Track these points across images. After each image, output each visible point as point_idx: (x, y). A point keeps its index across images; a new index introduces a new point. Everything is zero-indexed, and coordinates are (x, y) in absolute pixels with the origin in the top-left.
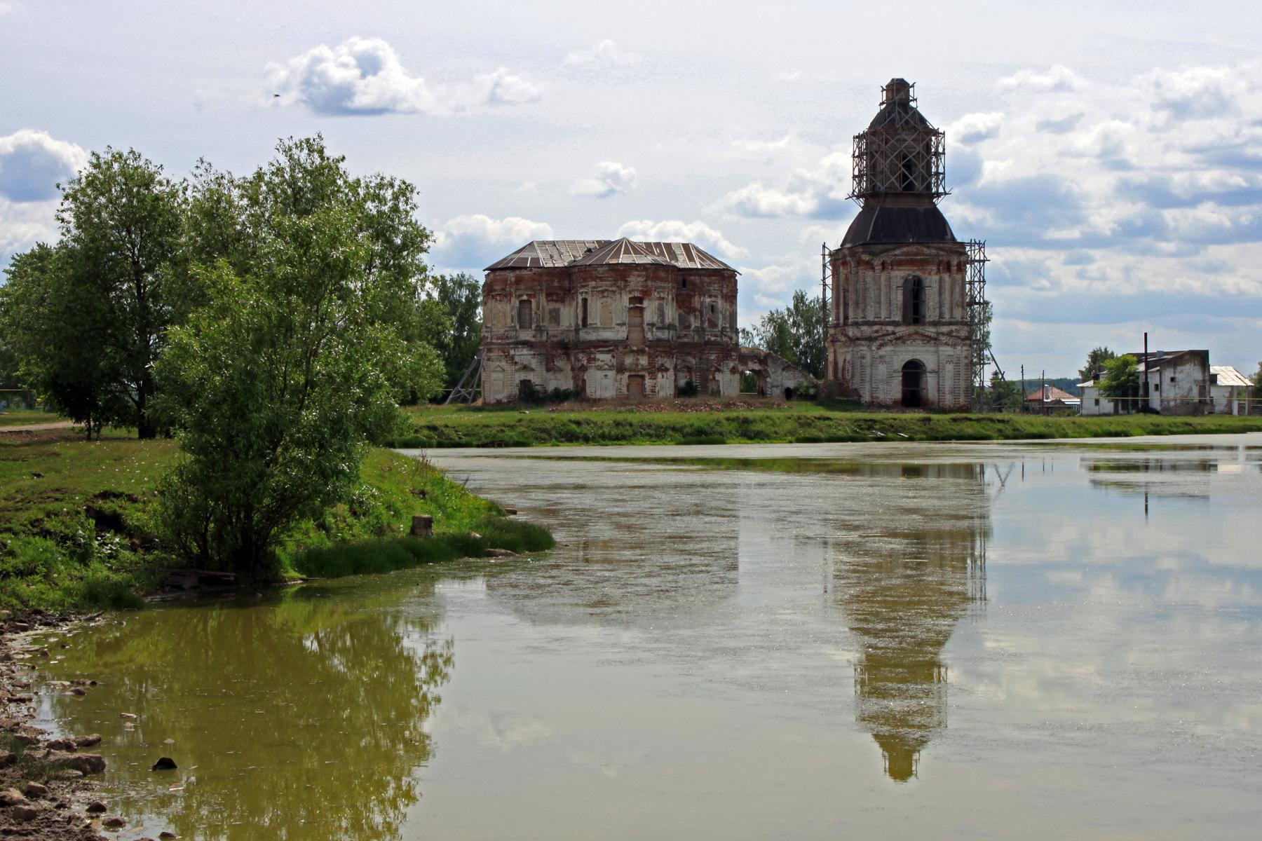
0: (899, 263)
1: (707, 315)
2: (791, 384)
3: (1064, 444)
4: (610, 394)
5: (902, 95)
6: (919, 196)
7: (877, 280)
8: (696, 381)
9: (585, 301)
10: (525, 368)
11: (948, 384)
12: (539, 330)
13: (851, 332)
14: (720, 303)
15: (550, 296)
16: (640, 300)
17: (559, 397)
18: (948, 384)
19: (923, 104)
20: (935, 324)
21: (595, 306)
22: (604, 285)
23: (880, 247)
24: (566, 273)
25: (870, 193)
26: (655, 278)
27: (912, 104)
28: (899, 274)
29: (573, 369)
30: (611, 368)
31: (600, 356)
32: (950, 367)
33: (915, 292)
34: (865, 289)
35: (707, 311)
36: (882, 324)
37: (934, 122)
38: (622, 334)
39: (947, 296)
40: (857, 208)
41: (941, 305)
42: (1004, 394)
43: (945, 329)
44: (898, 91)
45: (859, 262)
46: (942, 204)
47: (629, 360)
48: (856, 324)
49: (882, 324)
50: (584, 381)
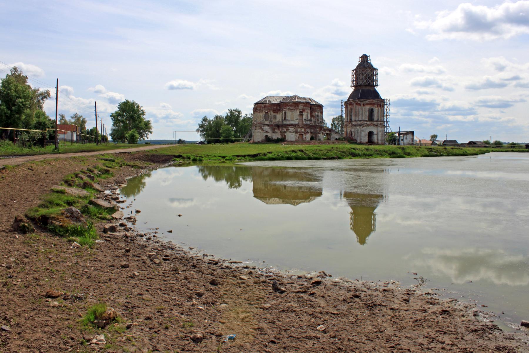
0: (367, 104)
1: (317, 117)
2: (337, 137)
3: (121, 146)
4: (293, 139)
5: (365, 59)
6: (371, 86)
7: (362, 109)
8: (314, 136)
9: (285, 113)
10: (267, 132)
11: (380, 138)
12: (271, 121)
13: (354, 123)
14: (320, 114)
15: (274, 111)
16: (302, 112)
17: (277, 141)
18: (380, 138)
19: (374, 61)
20: (377, 121)
21: (289, 114)
22: (291, 108)
23: (362, 100)
24: (279, 105)
25: (357, 86)
26: (306, 106)
27: (369, 61)
28: (368, 107)
29: (281, 132)
30: (294, 132)
31: (290, 128)
32: (380, 133)
33: (371, 112)
34: (359, 111)
35: (316, 117)
36: (363, 121)
37: (375, 66)
38: (297, 122)
39: (380, 114)
40: (351, 90)
41: (378, 116)
42: (393, 139)
43: (379, 123)
44: (365, 58)
45: (357, 104)
46: (377, 89)
47: (299, 130)
48: (356, 121)
49: (363, 121)
50: (285, 136)
